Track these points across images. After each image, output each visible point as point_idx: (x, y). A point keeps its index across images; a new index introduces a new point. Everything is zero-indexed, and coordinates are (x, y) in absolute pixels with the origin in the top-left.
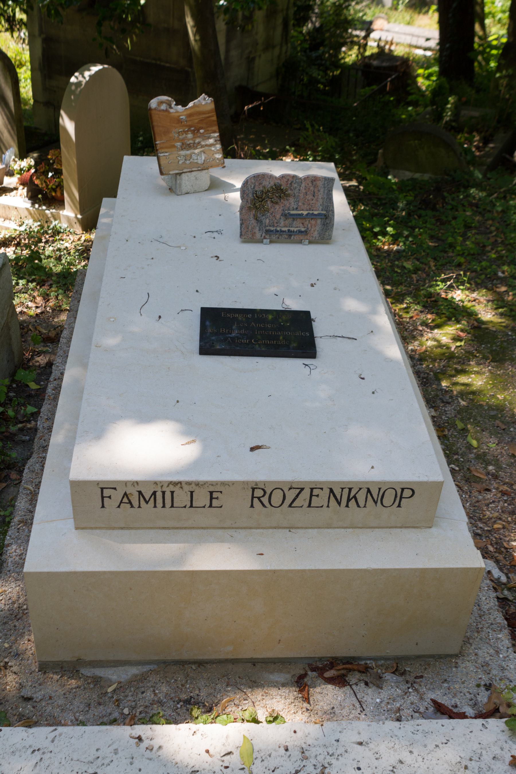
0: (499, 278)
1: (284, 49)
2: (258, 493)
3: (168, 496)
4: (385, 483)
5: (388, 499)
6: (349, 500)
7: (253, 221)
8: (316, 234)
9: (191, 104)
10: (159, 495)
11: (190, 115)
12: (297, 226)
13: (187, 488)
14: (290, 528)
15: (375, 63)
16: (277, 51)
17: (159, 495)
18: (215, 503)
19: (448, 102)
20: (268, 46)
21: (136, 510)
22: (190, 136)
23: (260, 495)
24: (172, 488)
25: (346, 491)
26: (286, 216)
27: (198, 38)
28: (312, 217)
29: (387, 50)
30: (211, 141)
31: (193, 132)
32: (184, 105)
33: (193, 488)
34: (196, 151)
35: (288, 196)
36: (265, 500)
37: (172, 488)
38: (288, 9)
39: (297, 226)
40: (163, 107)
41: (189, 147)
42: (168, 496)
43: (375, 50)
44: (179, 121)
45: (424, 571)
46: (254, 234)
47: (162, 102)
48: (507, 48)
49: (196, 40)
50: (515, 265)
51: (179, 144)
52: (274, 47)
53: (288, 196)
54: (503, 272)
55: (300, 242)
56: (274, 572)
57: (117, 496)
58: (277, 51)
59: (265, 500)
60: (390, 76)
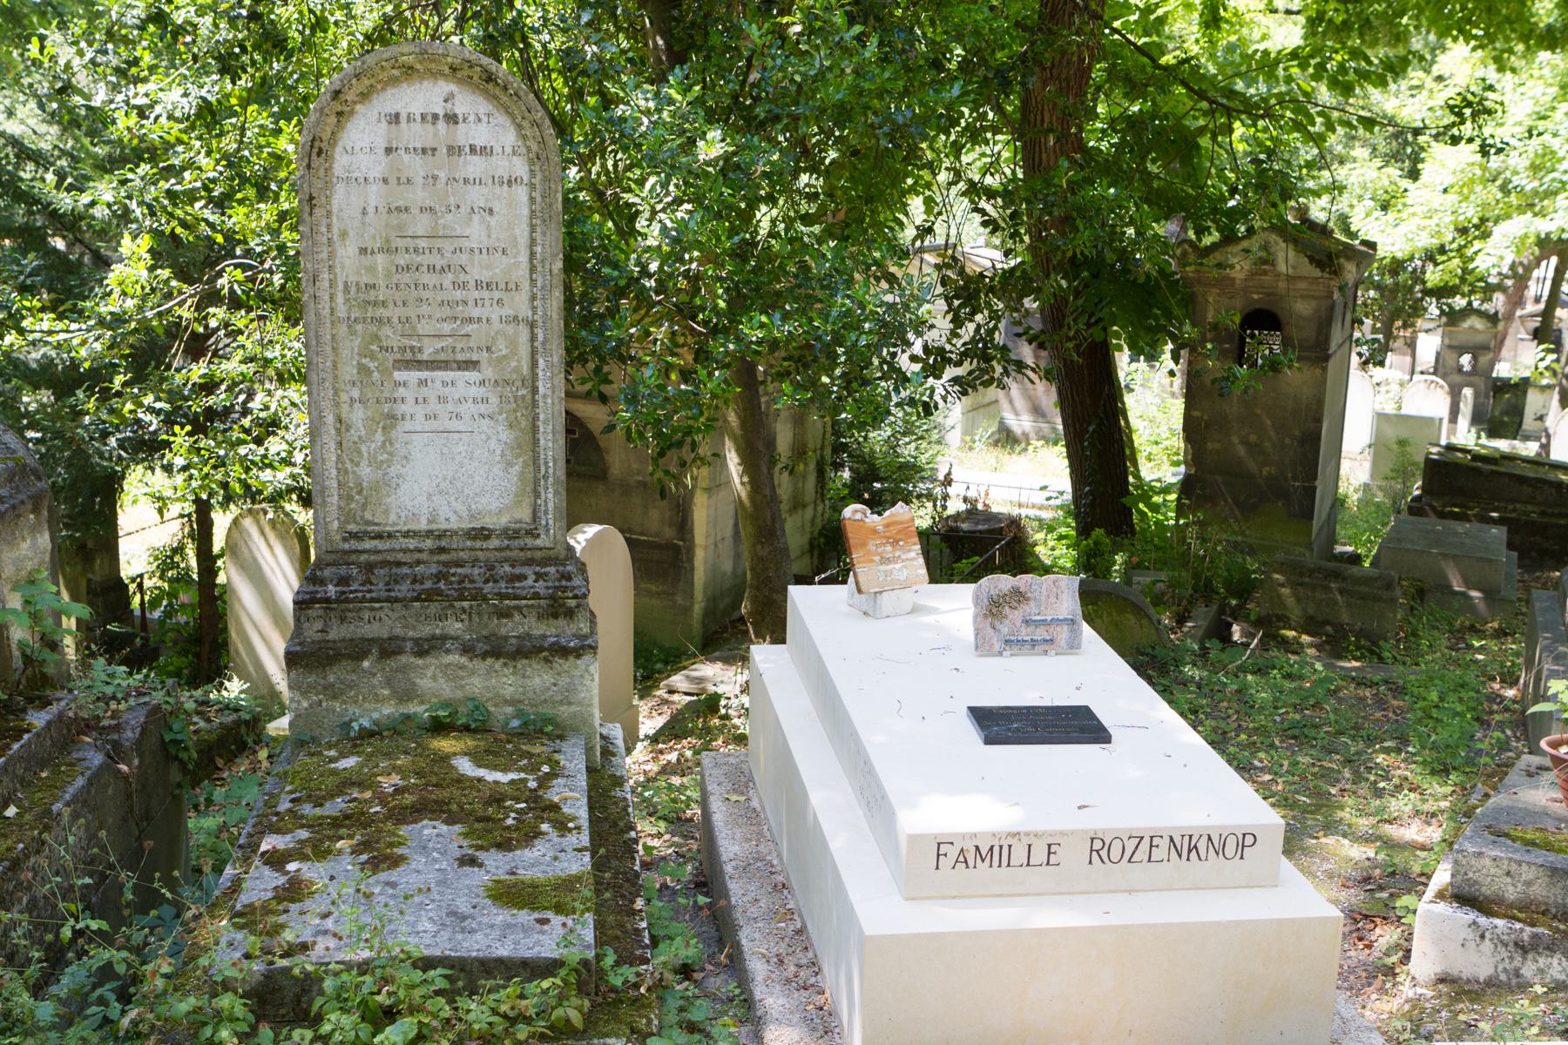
0: (1256, 768)
1: (820, 509)
2: (1097, 845)
3: (1005, 850)
4: (1226, 827)
5: (1230, 849)
6: (1190, 851)
7: (991, 631)
8: (1063, 643)
9: (887, 513)
10: (996, 850)
11: (887, 525)
12: (1041, 633)
13: (1026, 841)
14: (1129, 892)
15: (965, 526)
16: (809, 512)
17: (996, 850)
18: (1053, 859)
19: (1114, 563)
20: (797, 505)
21: (971, 870)
22: (889, 548)
23: (1099, 848)
24: (1010, 841)
25: (1186, 839)
26: (1027, 622)
27: (745, 479)
28: (1057, 621)
29: (980, 507)
30: (913, 554)
31: (892, 544)
32: (880, 514)
33: (1031, 840)
34: (898, 566)
35: (1028, 599)
36: (1104, 853)
37: (1010, 841)
38: (822, 449)
39: (1041, 633)
40: (858, 516)
41: (889, 561)
42: (1005, 850)
43: (963, 507)
44: (875, 532)
45: (1280, 922)
46: (991, 646)
47: (856, 511)
48: (1187, 487)
49: (742, 483)
50: (1524, 4)
51: (877, 558)
52: (804, 506)
53: (1028, 599)
54: (1261, 761)
55: (1046, 653)
56: (1125, 927)
57: (953, 852)
58: (809, 512)
59: (1104, 853)
60: (999, 541)
